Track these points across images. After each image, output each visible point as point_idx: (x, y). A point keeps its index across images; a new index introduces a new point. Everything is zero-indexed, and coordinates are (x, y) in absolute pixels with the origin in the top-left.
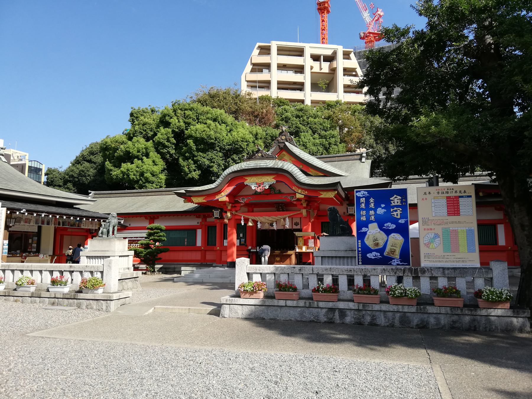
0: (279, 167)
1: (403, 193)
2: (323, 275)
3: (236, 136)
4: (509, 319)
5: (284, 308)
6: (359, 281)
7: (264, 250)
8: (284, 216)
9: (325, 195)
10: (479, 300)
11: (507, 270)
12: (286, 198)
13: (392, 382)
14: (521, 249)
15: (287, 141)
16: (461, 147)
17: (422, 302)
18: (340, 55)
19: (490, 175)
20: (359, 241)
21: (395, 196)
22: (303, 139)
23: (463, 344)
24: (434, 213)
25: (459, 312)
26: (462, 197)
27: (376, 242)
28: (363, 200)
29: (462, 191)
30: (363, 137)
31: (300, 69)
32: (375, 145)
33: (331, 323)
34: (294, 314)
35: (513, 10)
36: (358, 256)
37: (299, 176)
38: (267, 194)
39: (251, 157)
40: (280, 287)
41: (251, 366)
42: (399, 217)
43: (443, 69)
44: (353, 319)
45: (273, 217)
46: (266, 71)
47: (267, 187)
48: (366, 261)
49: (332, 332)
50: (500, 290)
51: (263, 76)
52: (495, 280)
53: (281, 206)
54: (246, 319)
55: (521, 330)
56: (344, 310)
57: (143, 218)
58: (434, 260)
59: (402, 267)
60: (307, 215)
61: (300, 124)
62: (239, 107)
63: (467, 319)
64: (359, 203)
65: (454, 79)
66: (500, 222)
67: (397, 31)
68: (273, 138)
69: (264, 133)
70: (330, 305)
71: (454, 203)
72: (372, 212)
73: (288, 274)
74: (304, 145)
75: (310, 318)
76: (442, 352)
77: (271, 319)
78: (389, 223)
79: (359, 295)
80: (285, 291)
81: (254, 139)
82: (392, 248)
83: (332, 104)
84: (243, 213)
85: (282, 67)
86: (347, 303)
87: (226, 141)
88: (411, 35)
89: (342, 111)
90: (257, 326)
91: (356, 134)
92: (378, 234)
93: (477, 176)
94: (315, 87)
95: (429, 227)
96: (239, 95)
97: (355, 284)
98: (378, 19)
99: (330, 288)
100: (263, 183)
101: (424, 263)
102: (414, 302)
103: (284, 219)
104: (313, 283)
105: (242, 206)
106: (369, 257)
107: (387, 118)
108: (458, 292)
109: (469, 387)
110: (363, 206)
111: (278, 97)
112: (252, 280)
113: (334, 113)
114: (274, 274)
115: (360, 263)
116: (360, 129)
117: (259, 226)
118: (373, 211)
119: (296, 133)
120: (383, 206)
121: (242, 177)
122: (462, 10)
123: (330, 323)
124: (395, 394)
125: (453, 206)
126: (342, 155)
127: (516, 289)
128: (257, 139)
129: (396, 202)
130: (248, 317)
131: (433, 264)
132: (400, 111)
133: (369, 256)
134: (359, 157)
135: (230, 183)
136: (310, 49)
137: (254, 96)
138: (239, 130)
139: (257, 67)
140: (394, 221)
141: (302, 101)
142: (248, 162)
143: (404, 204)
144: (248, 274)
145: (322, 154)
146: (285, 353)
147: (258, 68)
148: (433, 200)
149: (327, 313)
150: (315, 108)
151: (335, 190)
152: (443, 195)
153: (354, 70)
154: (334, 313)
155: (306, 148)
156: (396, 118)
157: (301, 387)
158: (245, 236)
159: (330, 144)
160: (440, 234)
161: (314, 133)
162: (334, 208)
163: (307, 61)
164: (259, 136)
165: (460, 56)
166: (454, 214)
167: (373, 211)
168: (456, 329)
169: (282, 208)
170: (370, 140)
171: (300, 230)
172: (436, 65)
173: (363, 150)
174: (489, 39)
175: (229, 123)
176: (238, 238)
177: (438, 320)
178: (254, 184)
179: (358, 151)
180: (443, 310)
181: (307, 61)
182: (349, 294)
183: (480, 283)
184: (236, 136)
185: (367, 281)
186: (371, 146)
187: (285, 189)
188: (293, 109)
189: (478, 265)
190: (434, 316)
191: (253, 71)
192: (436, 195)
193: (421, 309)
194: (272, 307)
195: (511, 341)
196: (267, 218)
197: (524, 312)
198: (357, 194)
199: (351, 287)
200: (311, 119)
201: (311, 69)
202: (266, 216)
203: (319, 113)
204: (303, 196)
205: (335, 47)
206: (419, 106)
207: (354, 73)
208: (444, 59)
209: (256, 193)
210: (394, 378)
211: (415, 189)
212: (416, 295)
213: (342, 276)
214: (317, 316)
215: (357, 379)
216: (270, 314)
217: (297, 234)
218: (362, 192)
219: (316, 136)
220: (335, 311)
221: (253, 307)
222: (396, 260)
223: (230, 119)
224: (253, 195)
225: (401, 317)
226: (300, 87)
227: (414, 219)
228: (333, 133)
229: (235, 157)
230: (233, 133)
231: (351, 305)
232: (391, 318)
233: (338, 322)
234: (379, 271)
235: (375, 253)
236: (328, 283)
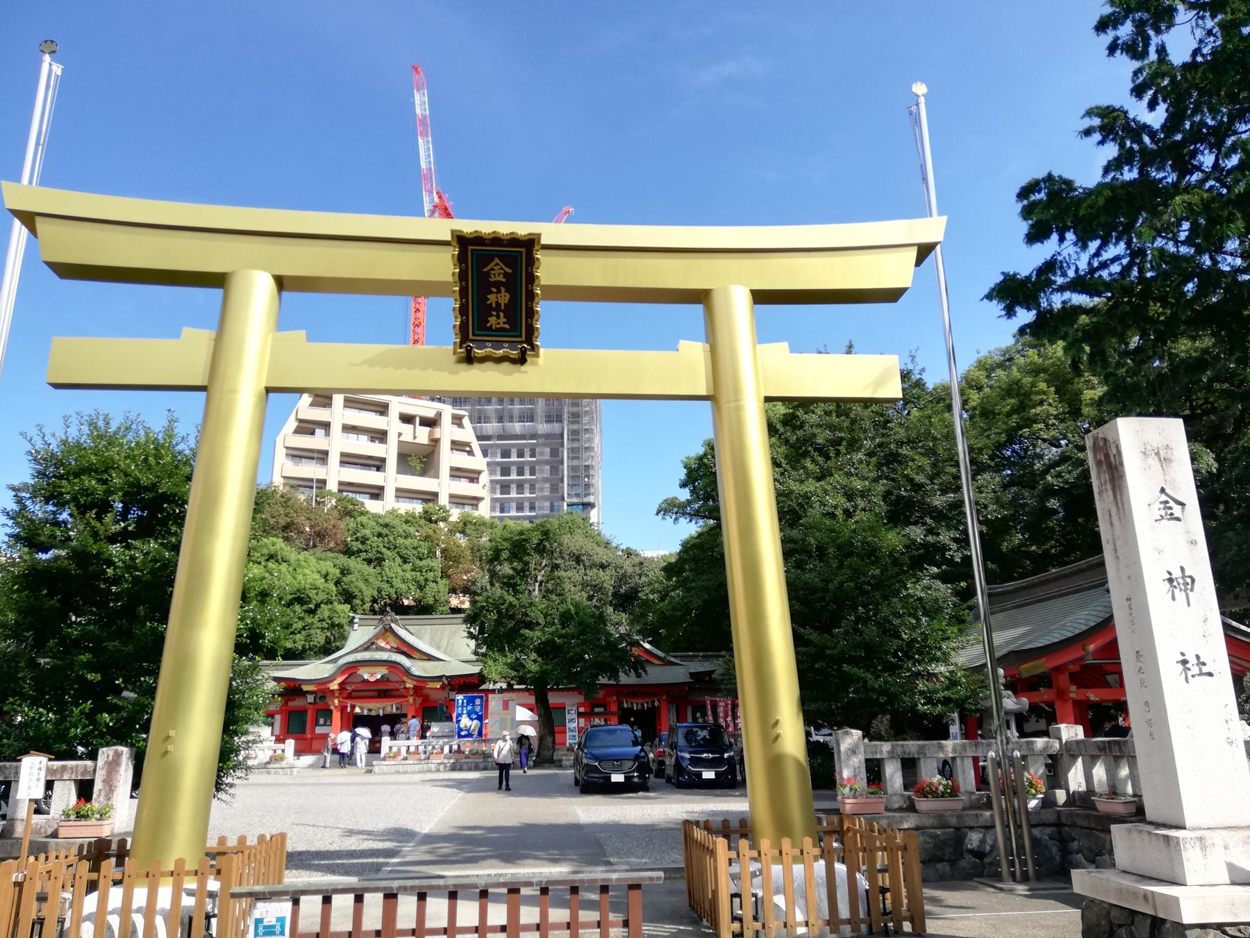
6: (455, 747)
9: (431, 685)
18: (446, 420)
31: (380, 436)
46: (320, 432)
48: (460, 736)
51: (316, 441)
135: (343, 673)
136: (398, 405)
140: (476, 713)
147: (306, 427)
159: (426, 580)
163: (391, 424)
181: (391, 424)
191: (298, 431)
200: (401, 541)
219: (408, 567)
226: (378, 464)
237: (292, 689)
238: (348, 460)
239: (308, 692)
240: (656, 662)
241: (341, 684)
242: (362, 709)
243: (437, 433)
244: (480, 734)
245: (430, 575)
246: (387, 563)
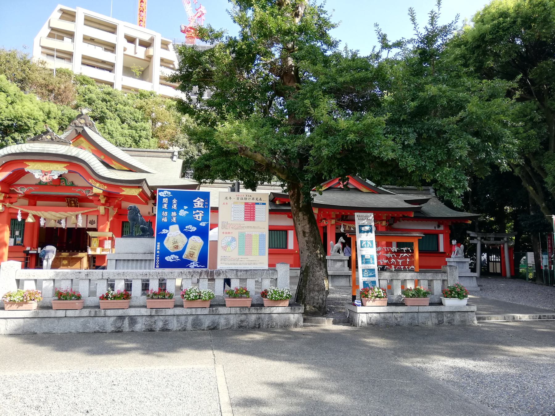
0: (73, 155)
1: (206, 196)
2: (114, 280)
3: (20, 110)
4: (286, 316)
5: (63, 320)
6: (154, 286)
7: (46, 252)
8: (77, 213)
10: (264, 299)
11: (289, 272)
12: (80, 192)
13: (174, 388)
14: (302, 253)
15: (87, 126)
16: (259, 157)
17: (215, 304)
18: (157, 43)
19: (282, 186)
20: (159, 243)
21: (198, 198)
22: (110, 127)
23: (247, 342)
24: (232, 218)
25: (247, 311)
26: (258, 204)
27: (176, 244)
28: (165, 200)
29: (259, 199)
30: (177, 134)
31: (111, 48)
32: (188, 145)
33: (119, 332)
34: (75, 326)
35: (311, 39)
36: (156, 259)
38: (56, 186)
39: (37, 138)
40: (60, 296)
41: (7, 392)
42: (200, 220)
43: (251, 81)
44: (144, 326)
45: (62, 213)
46: (67, 40)
47: (56, 177)
48: (163, 264)
49: (118, 341)
50: (282, 290)
51: (65, 45)
52: (279, 281)
53: (74, 201)
54: (11, 335)
55: (296, 325)
56: (134, 317)
57: (65, 203)
58: (230, 262)
59: (199, 270)
60: (105, 213)
61: (107, 109)
62: (27, 76)
63: (253, 318)
64: (161, 203)
65: (259, 92)
67: (211, 32)
68: (71, 120)
69: (60, 113)
70: (120, 313)
71: (251, 209)
72: (174, 214)
73: (72, 280)
74: (109, 134)
75: (94, 329)
76: (227, 351)
77: (44, 333)
78: (190, 226)
79: (153, 300)
80: (66, 299)
81: (46, 117)
82: (191, 250)
83: (145, 93)
84: (21, 206)
85: (89, 40)
86: (139, 309)
87: (6, 114)
88: (224, 39)
89: (158, 104)
90: (24, 343)
91: (169, 131)
92: (179, 236)
93: (273, 185)
94: (127, 71)
95: (227, 231)
96: (28, 61)
97: (150, 289)
98: (201, 16)
99: (121, 294)
100: (50, 172)
101: (221, 266)
102: (208, 304)
103: (77, 216)
104: (102, 289)
105: (20, 198)
106: (168, 260)
107: (197, 119)
108: (247, 293)
109: (245, 383)
110: (165, 206)
111: (81, 73)
112: (23, 288)
113: (147, 104)
114: (54, 280)
115: (157, 266)
116: (174, 126)
117: (42, 223)
118: (175, 213)
119: (101, 119)
120: (186, 207)
121: (22, 162)
122: (270, 28)
123: (118, 331)
124: (175, 400)
125: (250, 213)
126: (152, 150)
127: (296, 288)
128: (49, 118)
129: (199, 205)
130: (14, 332)
131: (228, 266)
132: (210, 114)
133: (168, 259)
134: (170, 155)
137: (48, 66)
138: (25, 103)
139: (56, 33)
140: (196, 223)
141: (112, 85)
142: (32, 145)
143: (206, 208)
144: (18, 281)
145: (131, 147)
146: (57, 371)
148: (233, 205)
149: (115, 321)
150: (126, 95)
151: (139, 187)
152: (242, 201)
153: (171, 62)
154: (123, 321)
155: (112, 137)
156: (205, 121)
157: (69, 408)
158: (22, 234)
160: (237, 238)
161: (123, 122)
162: (135, 207)
164: (52, 115)
165: (267, 72)
166: (250, 219)
167: (175, 213)
168: (243, 328)
169: (75, 203)
170: (183, 138)
171: (95, 230)
172: (245, 75)
173: (176, 149)
174: (291, 62)
175: (12, 93)
176: (12, 235)
177: (228, 320)
178: (38, 172)
179: (171, 149)
180: (233, 311)
181: (118, 39)
182: (143, 300)
183: (267, 285)
184: (20, 110)
185: (162, 284)
186: (184, 146)
187: (79, 181)
188: (98, 90)
189: (266, 267)
190: (225, 316)
191: (50, 36)
192: (236, 200)
193: (213, 311)
194: (47, 319)
195: (287, 336)
196: (53, 213)
197: (299, 309)
198: (160, 194)
199: (146, 292)
200: (120, 106)
201: (124, 50)
202: (53, 211)
203: (130, 101)
204: (101, 192)
205: (153, 33)
206: (225, 112)
207: (171, 66)
208: (254, 71)
209: (40, 184)
210: (176, 383)
211: (218, 192)
212: (210, 298)
213: (135, 280)
214: (104, 326)
215: (137, 390)
216: (45, 327)
217: (91, 234)
218: (165, 192)
219: (125, 125)
220: (124, 318)
221: (22, 320)
222: (193, 263)
223: (13, 88)
224: (36, 185)
225: (194, 320)
227: (214, 222)
228: (144, 125)
229: (16, 135)
230: (17, 107)
231: (144, 311)
232: (183, 322)
233: (127, 330)
234: (176, 274)
235: (173, 255)
236: (119, 289)
238: (88, 61)
240: (364, 190)
243: (151, 51)
244: (203, 260)
245: (143, 133)
246: (108, 121)
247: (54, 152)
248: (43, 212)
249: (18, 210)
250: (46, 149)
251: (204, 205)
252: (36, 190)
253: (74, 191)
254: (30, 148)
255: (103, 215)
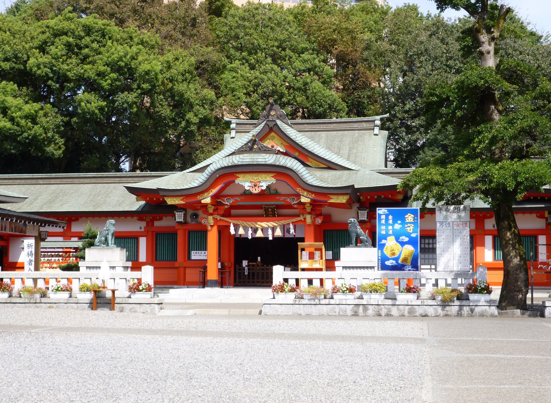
0: (281, 164)
12: (284, 200)
20: (380, 251)
28: (383, 217)
33: (357, 315)
37: (306, 176)
42: (411, 232)
66: (541, 232)
72: (390, 227)
92: (395, 246)
110: (383, 222)
115: (380, 269)
120: (399, 222)
224: (241, 195)
225: (410, 309)
237: (155, 205)
239: (175, 208)
241: (214, 197)
242: (236, 227)
247: (263, 163)
248: (248, 223)
249: (230, 223)
250: (255, 160)
251: (414, 220)
252: (242, 201)
253: (279, 200)
254: (241, 160)
255: (309, 225)
